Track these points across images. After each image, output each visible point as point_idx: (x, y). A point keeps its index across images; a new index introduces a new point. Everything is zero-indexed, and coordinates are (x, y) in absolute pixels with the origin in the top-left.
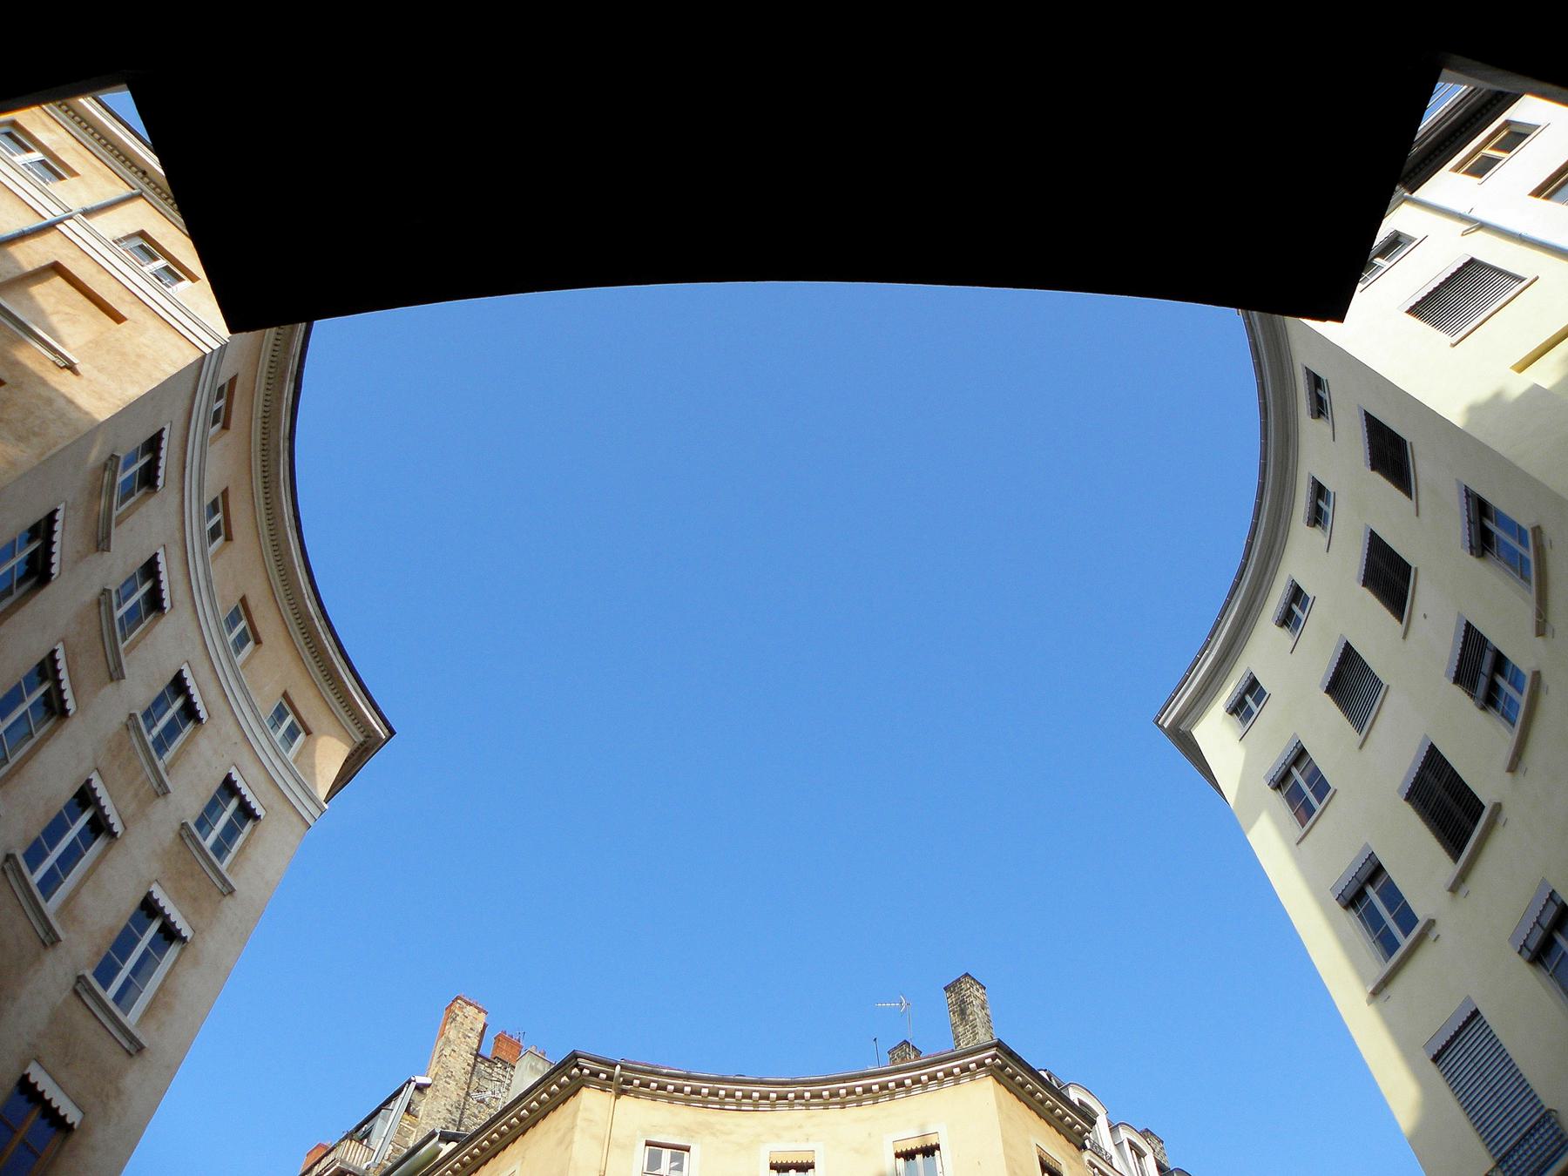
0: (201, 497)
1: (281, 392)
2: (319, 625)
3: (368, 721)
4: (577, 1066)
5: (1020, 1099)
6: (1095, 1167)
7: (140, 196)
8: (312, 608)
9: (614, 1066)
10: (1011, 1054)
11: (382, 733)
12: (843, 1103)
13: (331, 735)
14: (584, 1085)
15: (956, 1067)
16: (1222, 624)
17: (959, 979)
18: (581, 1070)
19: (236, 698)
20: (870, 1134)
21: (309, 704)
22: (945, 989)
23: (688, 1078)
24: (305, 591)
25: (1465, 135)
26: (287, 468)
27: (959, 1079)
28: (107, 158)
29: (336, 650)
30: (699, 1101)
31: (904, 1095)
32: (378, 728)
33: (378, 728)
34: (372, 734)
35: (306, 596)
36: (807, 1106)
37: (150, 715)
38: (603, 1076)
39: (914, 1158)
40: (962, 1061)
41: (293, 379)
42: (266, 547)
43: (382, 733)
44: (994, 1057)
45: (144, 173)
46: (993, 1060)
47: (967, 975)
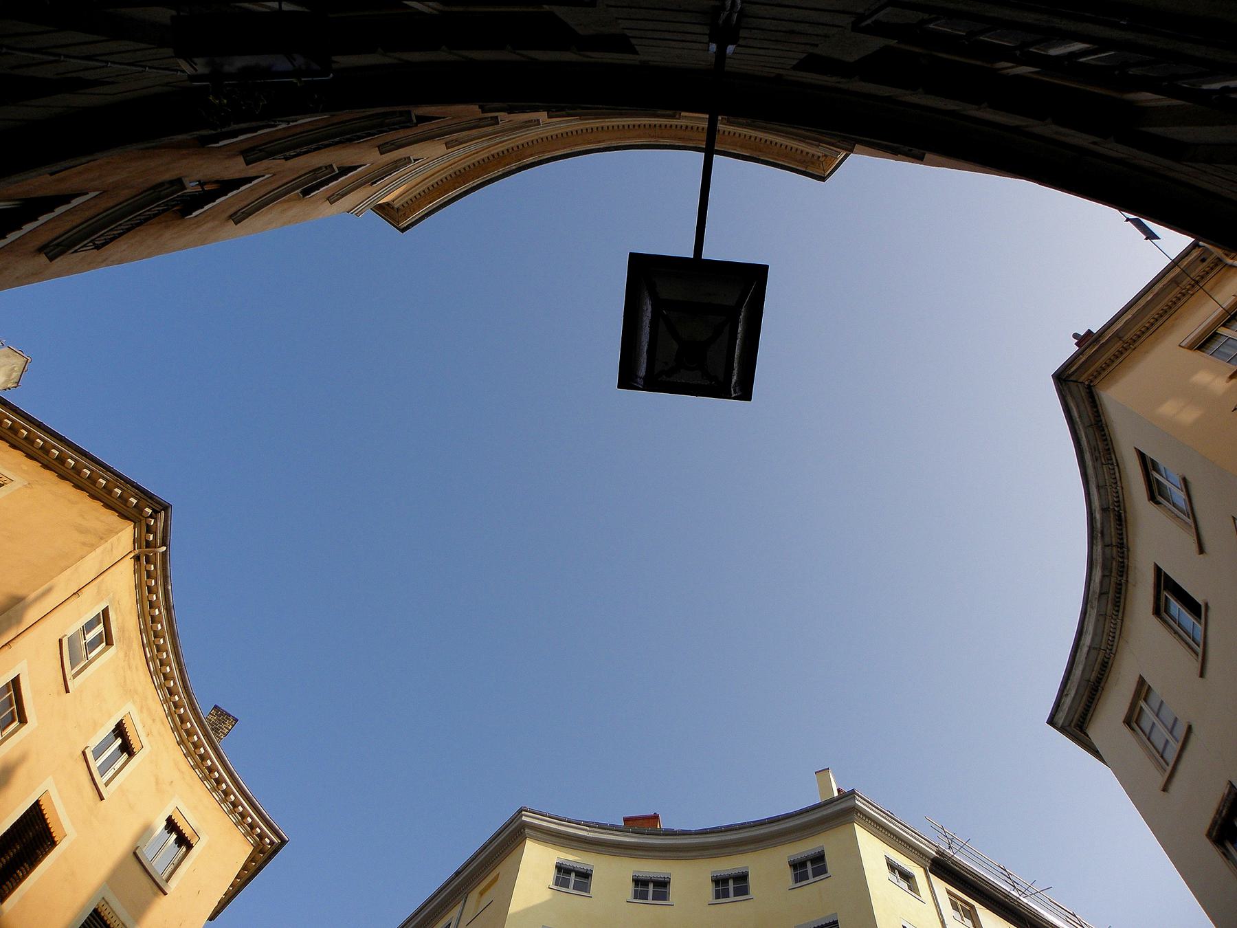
4: (155, 512)
11: (404, 224)
12: (183, 741)
14: (135, 523)
15: (252, 818)
16: (611, 832)
17: (230, 715)
18: (151, 516)
20: (172, 782)
22: (216, 707)
23: (168, 609)
25: (958, 884)
30: (145, 625)
36: (170, 714)
39: (170, 832)
40: (258, 820)
43: (404, 224)
44: (272, 843)
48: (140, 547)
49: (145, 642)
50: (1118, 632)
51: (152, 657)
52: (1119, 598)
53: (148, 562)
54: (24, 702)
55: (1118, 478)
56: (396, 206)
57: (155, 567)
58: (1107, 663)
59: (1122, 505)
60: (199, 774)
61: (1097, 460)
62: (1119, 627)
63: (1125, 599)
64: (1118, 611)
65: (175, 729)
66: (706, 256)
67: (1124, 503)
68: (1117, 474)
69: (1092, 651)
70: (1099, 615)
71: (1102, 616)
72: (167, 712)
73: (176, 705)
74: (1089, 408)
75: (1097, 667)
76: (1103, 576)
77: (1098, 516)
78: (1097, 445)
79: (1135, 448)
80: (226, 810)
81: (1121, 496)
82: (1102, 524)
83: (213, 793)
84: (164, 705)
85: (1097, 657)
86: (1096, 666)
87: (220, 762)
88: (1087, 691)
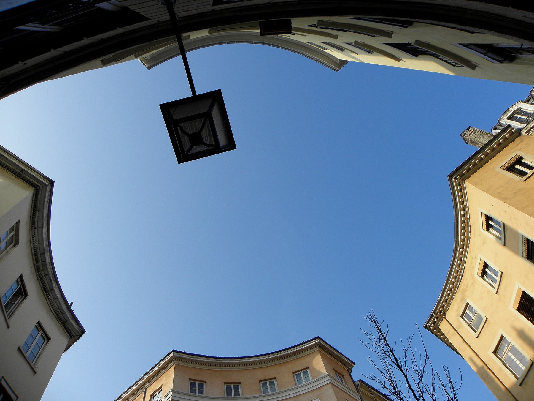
0: (219, 398)
1: (201, 361)
2: (277, 355)
3: (312, 345)
4: (430, 327)
5: (487, 162)
6: (530, 130)
7: (146, 389)
8: (272, 357)
9: (432, 316)
10: (457, 170)
13: (313, 360)
17: (463, 138)
18: (432, 326)
19: (281, 397)
21: (298, 365)
22: (467, 144)
24: (266, 358)
26: (226, 360)
27: (465, 193)
28: (138, 394)
29: (287, 351)
30: (455, 289)
31: (468, 215)
32: (315, 342)
33: (315, 342)
34: (317, 344)
35: (267, 358)
36: (466, 250)
37: (523, 174)
38: (435, 320)
41: (198, 357)
42: (252, 367)
43: (317, 341)
44: (456, 179)
45: (142, 386)
46: (457, 179)
47: (461, 135)
48: (440, 318)
49: (459, 282)
50: (32, 241)
51: (462, 270)
52: (35, 256)
53: (441, 311)
54: (498, 341)
55: (51, 307)
56: (318, 348)
57: (440, 308)
58: (32, 224)
59: (46, 296)
60: (469, 222)
61: (61, 309)
62: (32, 243)
63: (33, 257)
64: (34, 250)
65: (468, 244)
66: (198, 93)
67: (45, 297)
68: (51, 308)
69: (41, 226)
70: (42, 243)
71: (41, 243)
72: (467, 252)
73: (462, 253)
74: (70, 328)
75: (36, 220)
76: (45, 261)
77: (54, 285)
78: (62, 315)
79: (20, 220)
80: (467, 202)
81: (47, 299)
82: (52, 284)
83: (468, 211)
84: (466, 255)
85: (38, 224)
86: (37, 219)
87: (458, 222)
88: (38, 207)
